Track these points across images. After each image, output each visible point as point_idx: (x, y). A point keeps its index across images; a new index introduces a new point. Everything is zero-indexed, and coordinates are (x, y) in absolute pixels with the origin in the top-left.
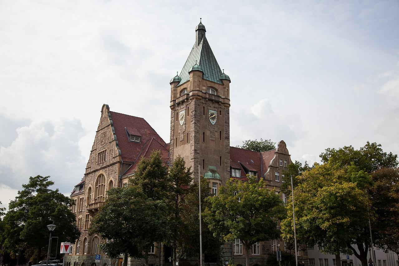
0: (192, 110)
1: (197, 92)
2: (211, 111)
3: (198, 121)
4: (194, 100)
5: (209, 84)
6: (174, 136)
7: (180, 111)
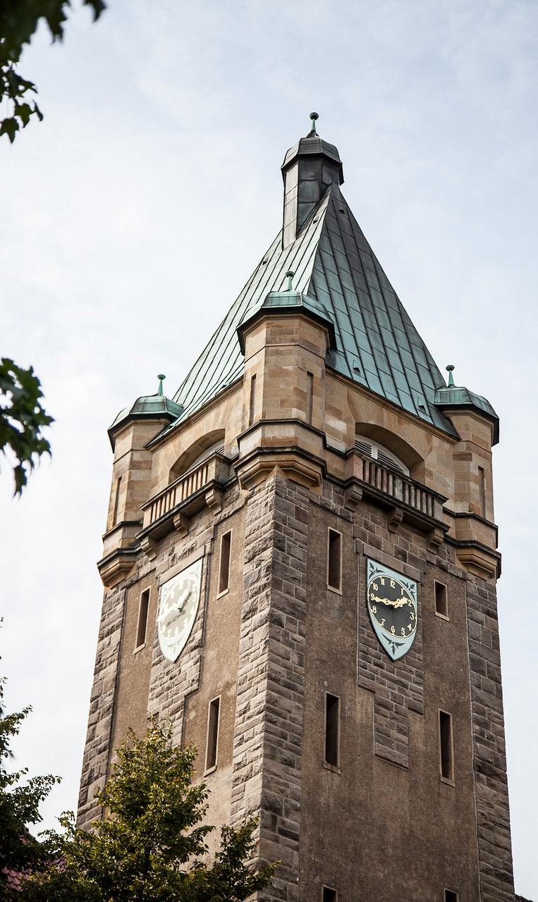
0: (249, 548)
1: (290, 432)
2: (379, 572)
3: (294, 610)
4: (271, 480)
5: (371, 414)
6: (109, 747)
7: (163, 578)
